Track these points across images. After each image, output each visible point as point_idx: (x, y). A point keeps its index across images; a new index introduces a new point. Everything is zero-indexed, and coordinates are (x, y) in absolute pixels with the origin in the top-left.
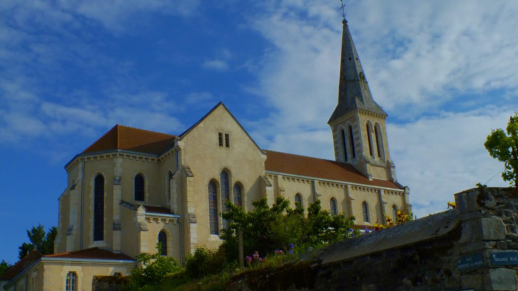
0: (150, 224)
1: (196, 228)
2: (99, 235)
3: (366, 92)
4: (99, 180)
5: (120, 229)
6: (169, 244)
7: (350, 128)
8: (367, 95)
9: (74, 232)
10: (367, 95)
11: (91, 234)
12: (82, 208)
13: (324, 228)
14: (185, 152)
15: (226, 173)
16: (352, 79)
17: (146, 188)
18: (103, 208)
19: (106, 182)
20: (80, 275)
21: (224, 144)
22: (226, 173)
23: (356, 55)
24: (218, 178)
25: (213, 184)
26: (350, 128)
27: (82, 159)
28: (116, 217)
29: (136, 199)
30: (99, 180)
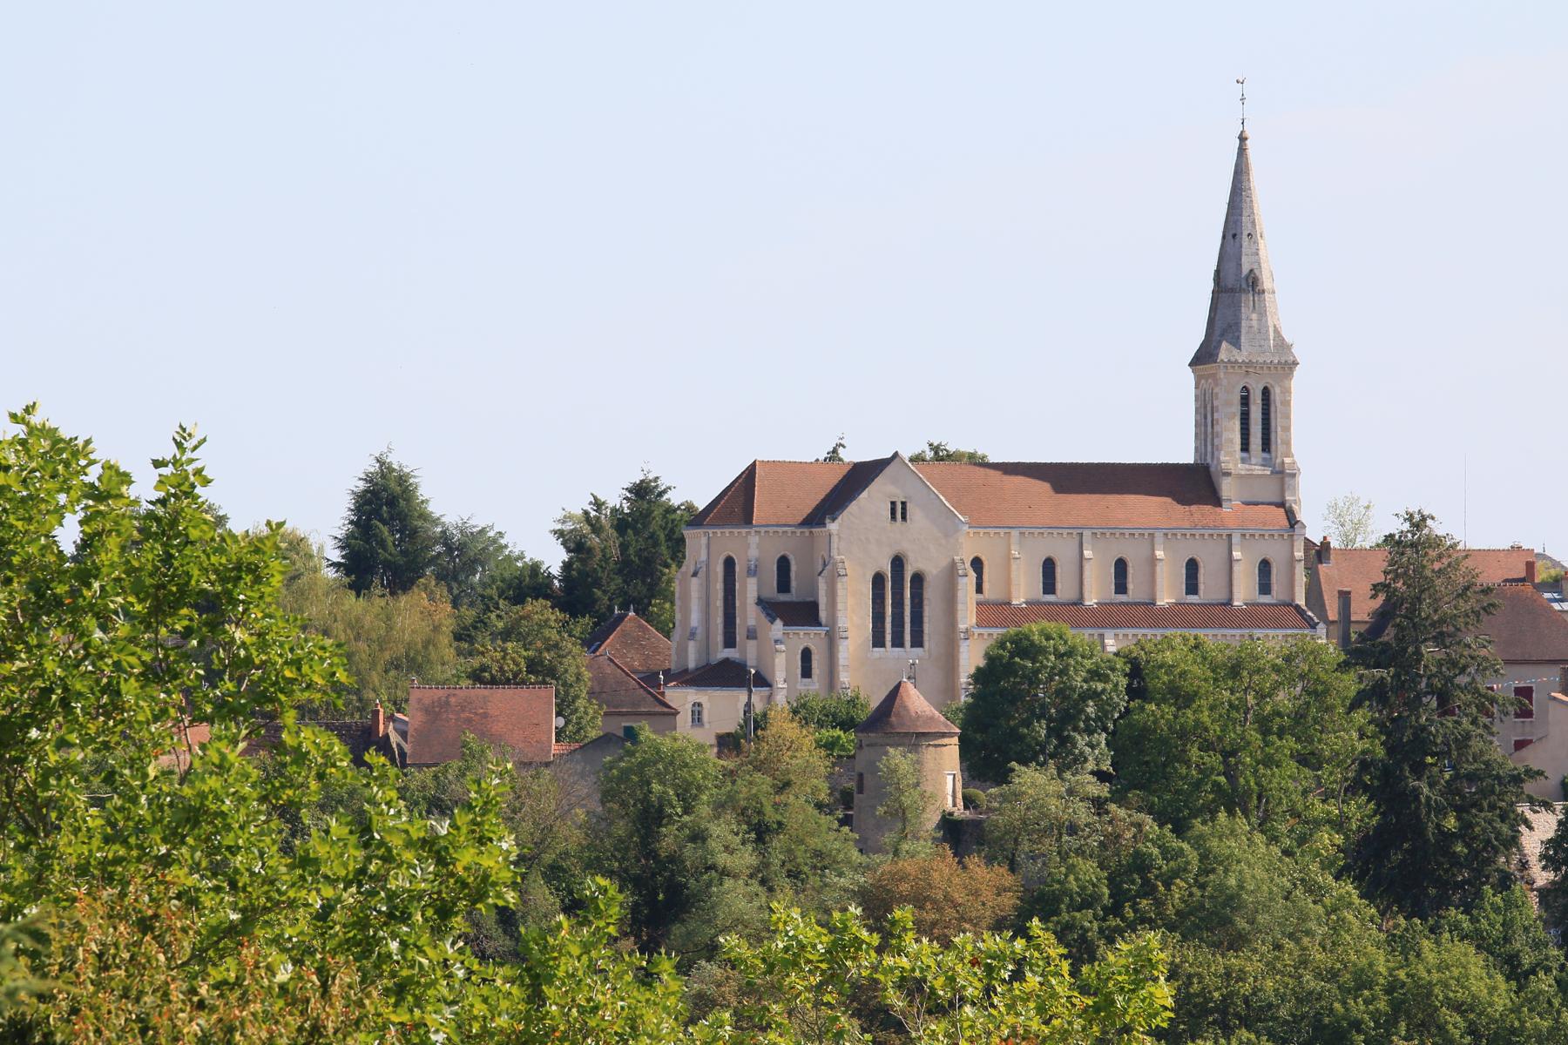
0: (1536, 815)
1: (341, 540)
2: (730, 641)
3: (1254, 316)
4: (729, 564)
5: (755, 638)
6: (815, 664)
7: (1266, 393)
8: (1255, 323)
9: (698, 637)
10: (1255, 323)
11: (720, 638)
12: (708, 604)
13: (556, 582)
14: (839, 538)
15: (898, 563)
16: (1230, 286)
17: (793, 575)
18: (734, 604)
19: (737, 568)
20: (706, 706)
21: (899, 507)
22: (898, 563)
23: (1249, 225)
24: (888, 570)
25: (878, 580)
26: (1266, 393)
27: (705, 533)
28: (751, 622)
29: (1044, 593)
30: (729, 564)
